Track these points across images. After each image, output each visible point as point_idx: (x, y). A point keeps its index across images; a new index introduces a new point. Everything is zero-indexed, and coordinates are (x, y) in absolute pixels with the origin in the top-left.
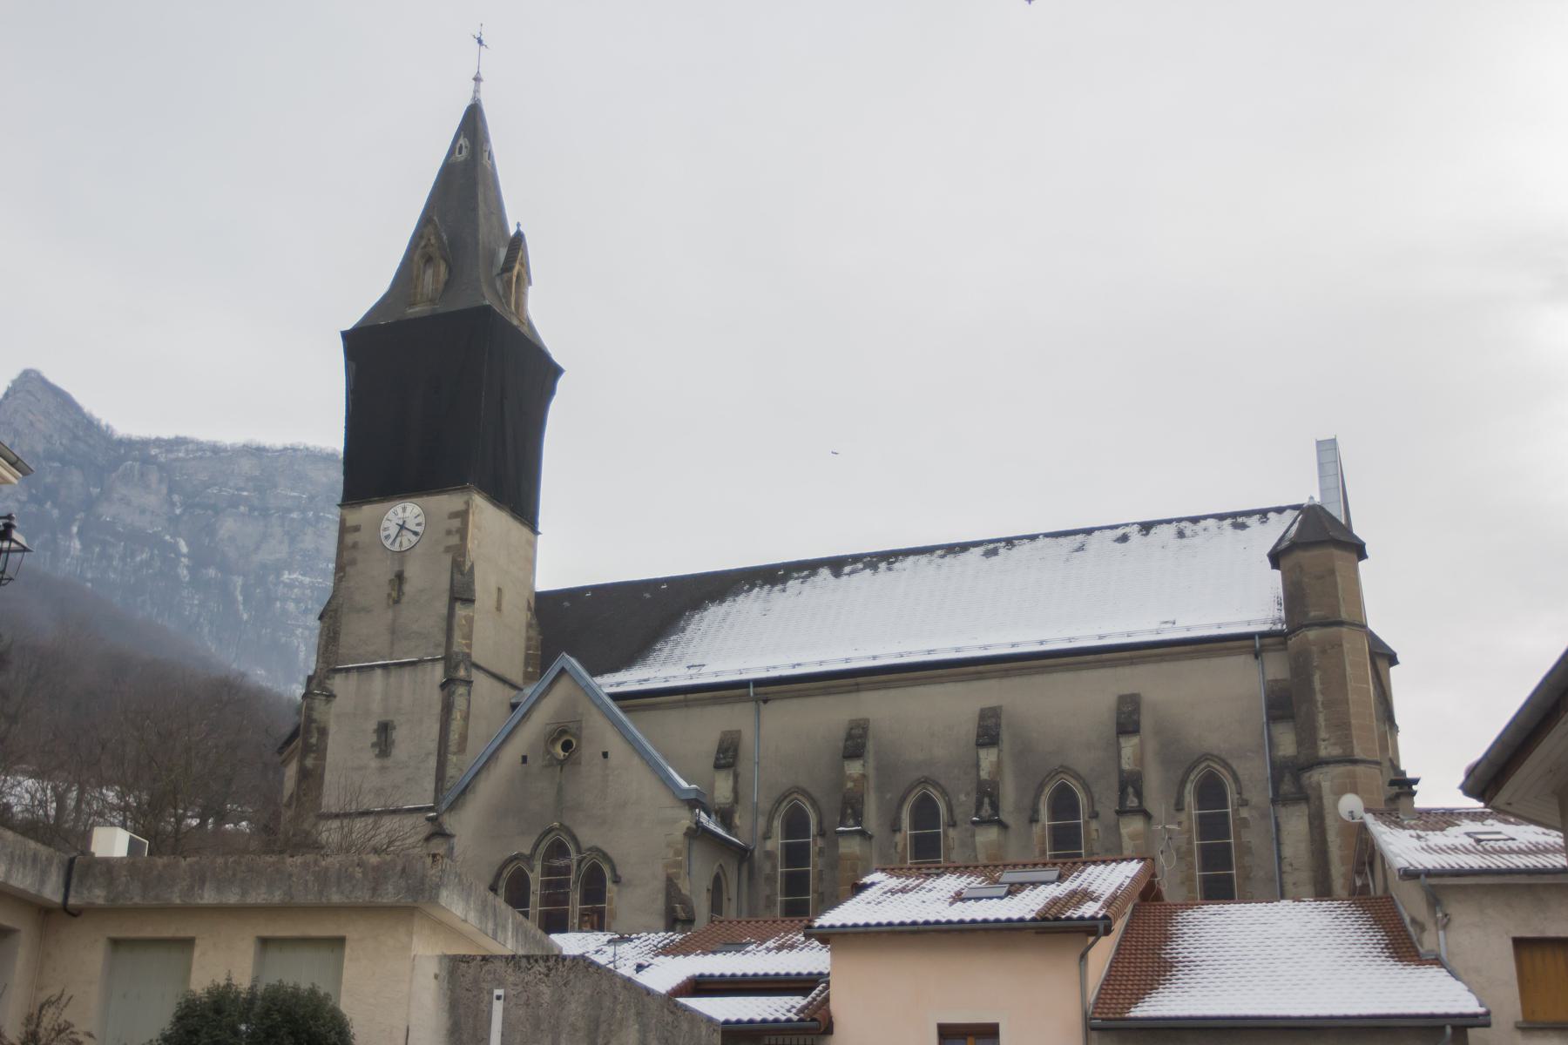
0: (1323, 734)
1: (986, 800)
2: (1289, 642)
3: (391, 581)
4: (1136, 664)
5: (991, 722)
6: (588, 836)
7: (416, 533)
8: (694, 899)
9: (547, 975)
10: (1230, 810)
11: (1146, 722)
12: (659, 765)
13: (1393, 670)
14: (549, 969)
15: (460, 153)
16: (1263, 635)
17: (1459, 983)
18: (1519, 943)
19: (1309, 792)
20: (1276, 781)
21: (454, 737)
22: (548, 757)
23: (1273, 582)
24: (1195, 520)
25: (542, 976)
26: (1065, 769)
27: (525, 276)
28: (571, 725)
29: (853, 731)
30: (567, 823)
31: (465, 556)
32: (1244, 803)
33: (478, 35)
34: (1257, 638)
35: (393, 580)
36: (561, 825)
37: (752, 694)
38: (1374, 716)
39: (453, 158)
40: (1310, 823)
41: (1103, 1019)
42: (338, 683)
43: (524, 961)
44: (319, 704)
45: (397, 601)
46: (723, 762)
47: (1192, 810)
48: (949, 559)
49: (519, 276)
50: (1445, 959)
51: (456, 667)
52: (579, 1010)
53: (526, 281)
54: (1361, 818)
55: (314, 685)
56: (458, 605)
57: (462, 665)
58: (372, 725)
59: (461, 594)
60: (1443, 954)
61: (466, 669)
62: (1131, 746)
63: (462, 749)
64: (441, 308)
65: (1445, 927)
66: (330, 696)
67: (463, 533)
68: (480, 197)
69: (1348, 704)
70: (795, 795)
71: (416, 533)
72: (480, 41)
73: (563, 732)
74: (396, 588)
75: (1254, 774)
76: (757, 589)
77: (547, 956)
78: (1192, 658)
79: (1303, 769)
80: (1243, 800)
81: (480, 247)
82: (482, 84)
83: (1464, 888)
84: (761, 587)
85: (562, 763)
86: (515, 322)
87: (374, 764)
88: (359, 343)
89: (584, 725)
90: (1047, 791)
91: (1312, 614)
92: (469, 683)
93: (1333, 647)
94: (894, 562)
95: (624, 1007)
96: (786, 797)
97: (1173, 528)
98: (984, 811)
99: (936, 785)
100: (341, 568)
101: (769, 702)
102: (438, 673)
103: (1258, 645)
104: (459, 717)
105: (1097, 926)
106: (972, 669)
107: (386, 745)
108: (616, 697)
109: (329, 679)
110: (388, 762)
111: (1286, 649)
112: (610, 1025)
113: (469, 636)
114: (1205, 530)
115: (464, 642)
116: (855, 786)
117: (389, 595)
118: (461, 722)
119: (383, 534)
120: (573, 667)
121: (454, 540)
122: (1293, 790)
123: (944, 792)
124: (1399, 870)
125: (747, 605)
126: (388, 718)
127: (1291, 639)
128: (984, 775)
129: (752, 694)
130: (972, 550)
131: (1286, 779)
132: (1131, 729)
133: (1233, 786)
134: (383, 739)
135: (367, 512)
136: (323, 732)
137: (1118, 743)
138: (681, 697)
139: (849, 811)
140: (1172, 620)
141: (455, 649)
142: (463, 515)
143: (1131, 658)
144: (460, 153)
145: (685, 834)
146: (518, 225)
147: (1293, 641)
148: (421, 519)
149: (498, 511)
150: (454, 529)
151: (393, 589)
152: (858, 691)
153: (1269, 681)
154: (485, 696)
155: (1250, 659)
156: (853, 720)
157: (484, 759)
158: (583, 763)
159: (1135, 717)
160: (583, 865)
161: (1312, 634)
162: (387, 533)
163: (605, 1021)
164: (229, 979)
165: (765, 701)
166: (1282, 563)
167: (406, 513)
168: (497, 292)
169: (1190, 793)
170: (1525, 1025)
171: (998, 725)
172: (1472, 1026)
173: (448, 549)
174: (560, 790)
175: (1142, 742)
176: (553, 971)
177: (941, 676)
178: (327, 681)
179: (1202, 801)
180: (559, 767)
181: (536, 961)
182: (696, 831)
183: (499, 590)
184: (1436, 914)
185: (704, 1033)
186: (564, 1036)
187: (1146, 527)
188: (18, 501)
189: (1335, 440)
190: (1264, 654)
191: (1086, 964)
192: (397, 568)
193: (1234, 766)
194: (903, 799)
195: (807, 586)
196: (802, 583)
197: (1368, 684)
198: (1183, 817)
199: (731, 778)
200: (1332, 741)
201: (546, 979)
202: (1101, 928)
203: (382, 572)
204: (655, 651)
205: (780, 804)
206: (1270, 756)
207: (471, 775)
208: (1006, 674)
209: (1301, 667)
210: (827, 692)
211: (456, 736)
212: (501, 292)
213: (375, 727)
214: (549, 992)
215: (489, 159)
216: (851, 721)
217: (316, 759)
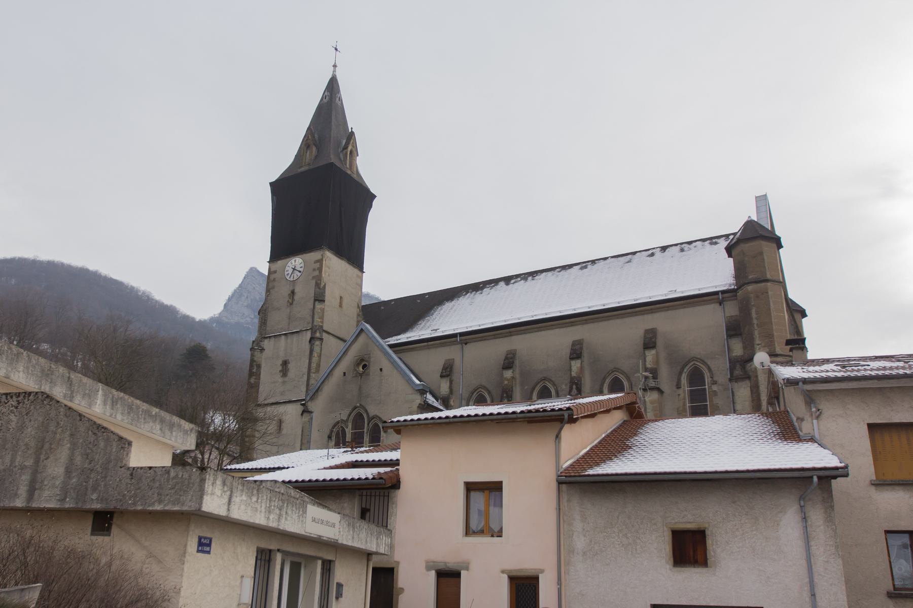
0: (757, 342)
1: (574, 387)
2: (738, 294)
3: (289, 295)
4: (655, 312)
5: (577, 347)
6: (373, 410)
7: (300, 272)
9: (16, 408)
10: (707, 387)
11: (660, 342)
12: (405, 374)
13: (804, 320)
14: (19, 403)
15: (325, 98)
16: (723, 292)
17: (826, 451)
18: (872, 427)
19: (750, 374)
20: (732, 369)
21: (314, 365)
22: (355, 372)
23: (728, 265)
24: (690, 243)
25: (13, 408)
26: (617, 370)
27: (355, 152)
28: (365, 356)
29: (509, 356)
30: (363, 404)
31: (321, 281)
32: (715, 383)
33: (335, 46)
34: (720, 293)
35: (290, 294)
36: (360, 405)
37: (458, 340)
38: (788, 332)
39: (322, 102)
40: (751, 391)
41: (566, 476)
42: (266, 344)
43: (4, 397)
44: (257, 354)
45: (291, 304)
46: (444, 374)
47: (686, 388)
48: (563, 272)
49: (351, 152)
50: (819, 439)
51: (315, 332)
52: (33, 433)
53: (356, 154)
54: (769, 366)
55: (255, 345)
56: (317, 303)
57: (318, 331)
58: (280, 362)
59: (319, 298)
60: (817, 436)
61: (320, 333)
62: (651, 355)
63: (318, 370)
64: (312, 167)
65: (818, 417)
66: (262, 350)
67: (320, 270)
68: (333, 117)
69: (772, 324)
70: (480, 389)
71: (300, 272)
72: (336, 49)
73: (362, 360)
74: (291, 298)
75: (720, 367)
76: (469, 294)
77: (19, 393)
78: (685, 308)
79: (746, 362)
80: (714, 381)
81: (332, 139)
82: (337, 68)
83: (831, 391)
84: (471, 293)
85: (361, 375)
86: (349, 172)
87: (280, 380)
88: (277, 187)
89: (371, 355)
90: (608, 381)
91: (750, 277)
92: (321, 339)
93: (763, 294)
94: (535, 276)
95: (62, 430)
96: (476, 390)
97: (678, 247)
98: (573, 392)
99: (550, 380)
100: (268, 290)
101: (468, 344)
102: (308, 335)
103: (721, 298)
104: (316, 356)
105: (563, 415)
106: (568, 321)
107: (286, 371)
108: (391, 346)
109: (261, 342)
110: (286, 379)
111: (737, 299)
112: (51, 444)
113: (322, 318)
114: (695, 247)
115: (319, 320)
116: (509, 383)
117: (288, 301)
118: (317, 358)
119: (286, 273)
120: (366, 328)
121: (317, 273)
122: (741, 373)
123: (554, 384)
124: (784, 380)
125: (463, 302)
126: (286, 359)
127: (739, 292)
128: (574, 374)
129: (458, 340)
130: (574, 267)
131: (737, 368)
132: (651, 346)
133: (708, 374)
134: (285, 368)
135: (280, 263)
136: (259, 366)
137: (644, 354)
138: (426, 344)
139: (505, 395)
140: (674, 290)
141: (315, 323)
142: (320, 261)
143: (651, 309)
144: (325, 98)
145: (418, 407)
146: (352, 128)
147: (740, 293)
148: (302, 265)
149: (340, 260)
150: (317, 268)
151: (290, 298)
152: (511, 335)
153: (727, 317)
154: (332, 347)
155: (717, 306)
156: (508, 351)
157: (326, 375)
158: (371, 373)
159: (653, 340)
160: (370, 424)
161: (750, 288)
162: (287, 273)
163: (48, 442)
165: (466, 344)
166: (733, 253)
167: (297, 262)
168: (340, 159)
169: (684, 378)
170: (878, 483)
171: (581, 348)
172: (835, 477)
173: (314, 278)
174: (360, 388)
175: (657, 353)
176: (21, 404)
177: (552, 325)
178: (261, 343)
179: (691, 383)
180: (360, 377)
181: (12, 397)
182: (423, 405)
183: (341, 297)
184: (811, 409)
185: (114, 450)
186: (20, 453)
187: (664, 249)
188: (250, 318)
189: (766, 195)
190: (724, 303)
191: (559, 442)
192: (291, 288)
193: (709, 363)
194: (533, 389)
195: (493, 290)
196: (491, 289)
197: (784, 314)
198: (681, 391)
199: (448, 382)
200: (763, 345)
201: (15, 410)
202: (566, 416)
203: (285, 291)
204: (418, 324)
205: (473, 394)
206: (729, 357)
207: (320, 382)
208: (586, 322)
209: (745, 308)
210: (495, 337)
211: (315, 365)
212: (342, 159)
213: (281, 363)
214: (15, 420)
215: (339, 100)
216: (507, 351)
217: (255, 379)
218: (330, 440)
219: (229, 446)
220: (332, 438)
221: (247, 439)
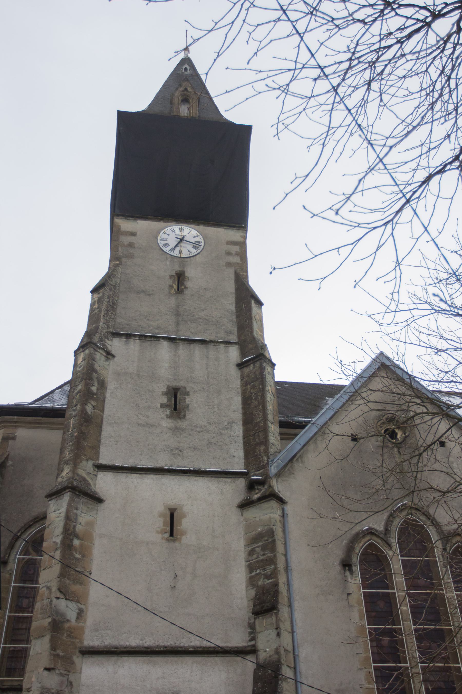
8: (131, 644)
35: (173, 276)
58: (161, 388)
87: (166, 423)
136: (102, 385)
151: (174, 282)
164: (83, 659)
192: (177, 268)
211: (271, 407)
213: (165, 390)
218: (348, 573)
219: (78, 407)
220: (354, 568)
221: (76, 542)
